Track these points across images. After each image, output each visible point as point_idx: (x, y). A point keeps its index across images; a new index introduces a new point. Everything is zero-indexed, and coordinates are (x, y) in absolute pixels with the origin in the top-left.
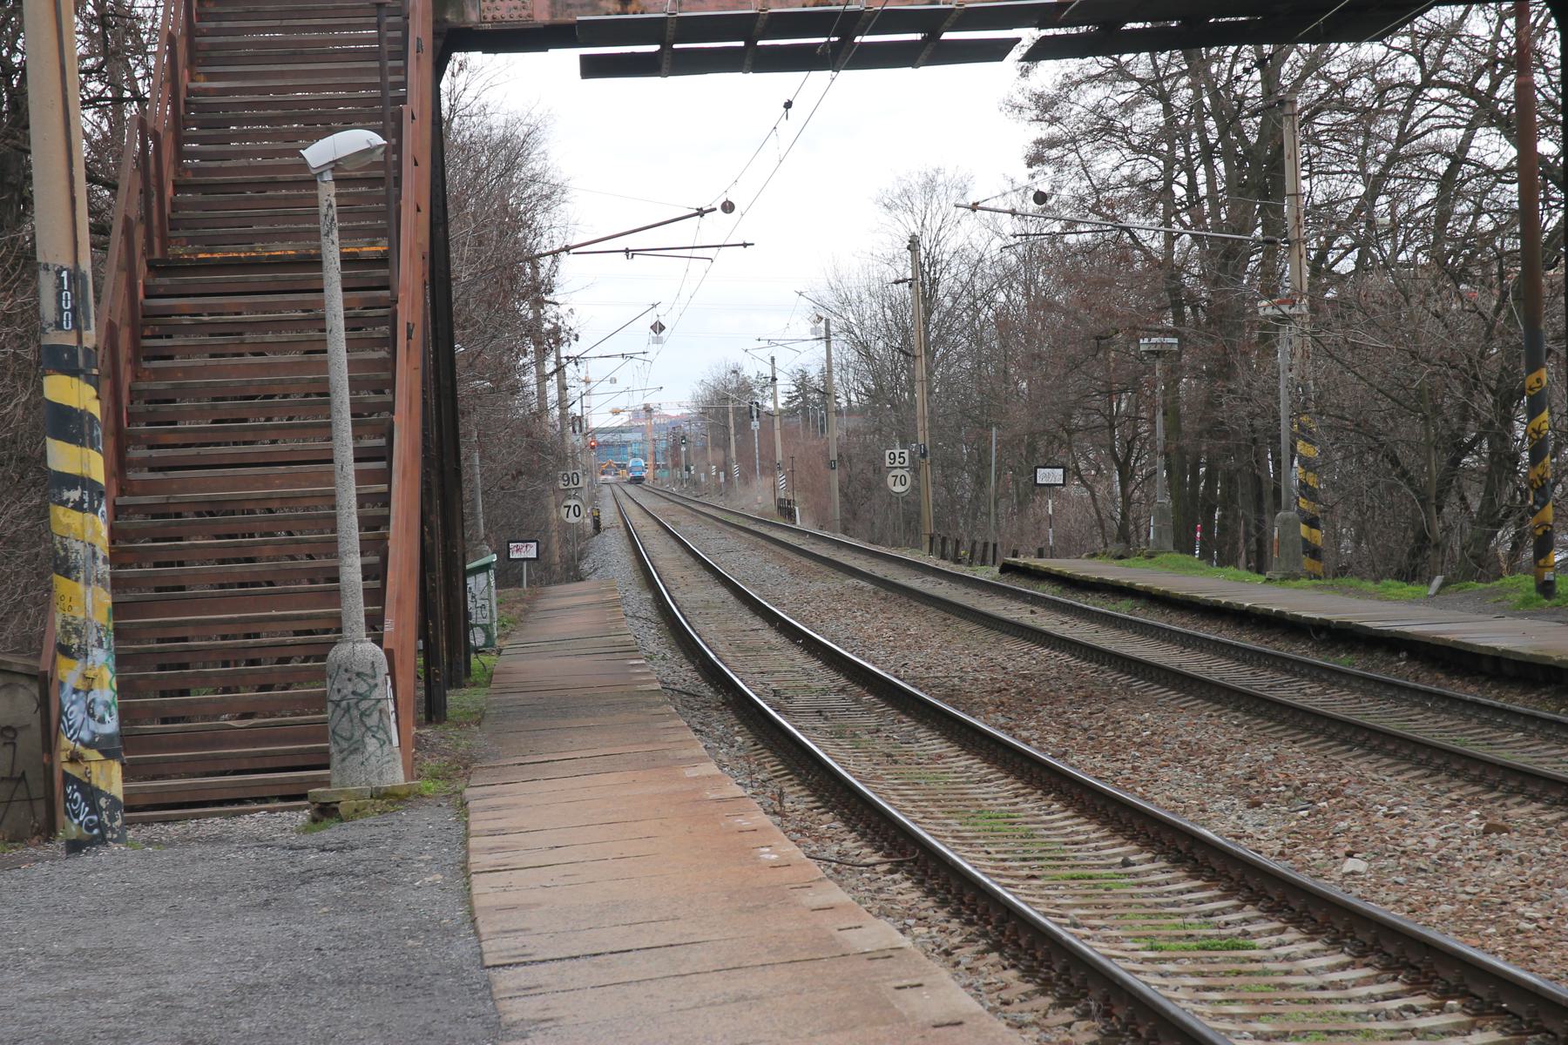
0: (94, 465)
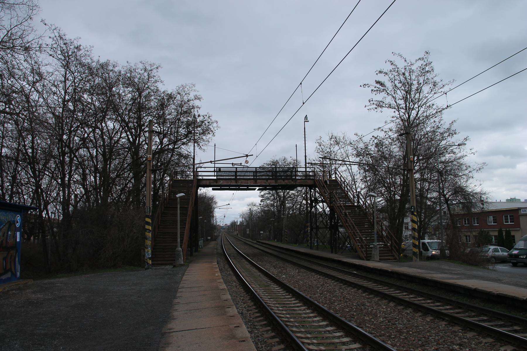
0: (150, 228)
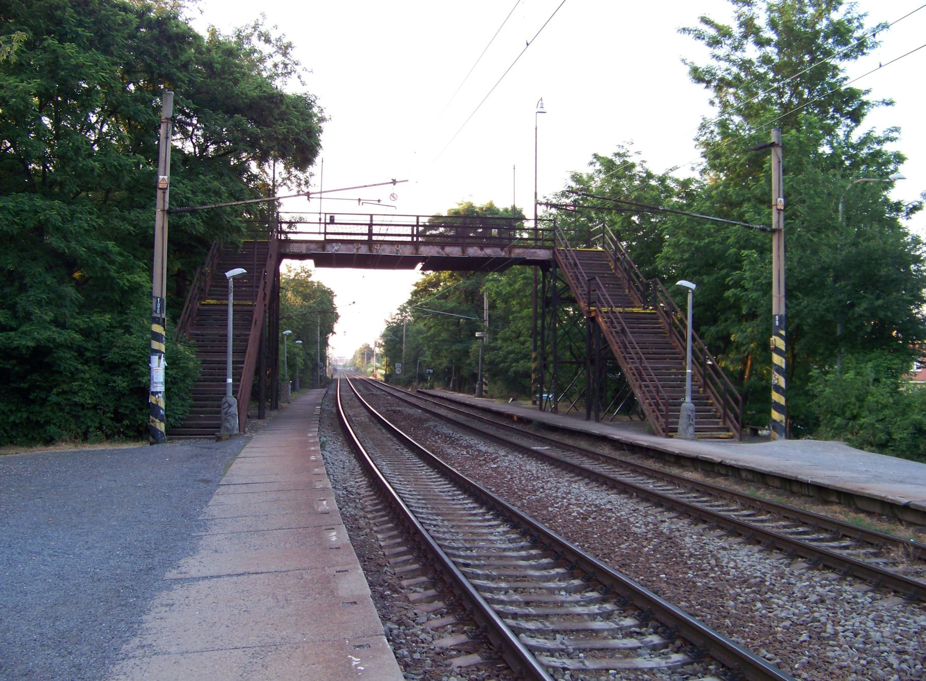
0: (163, 348)
